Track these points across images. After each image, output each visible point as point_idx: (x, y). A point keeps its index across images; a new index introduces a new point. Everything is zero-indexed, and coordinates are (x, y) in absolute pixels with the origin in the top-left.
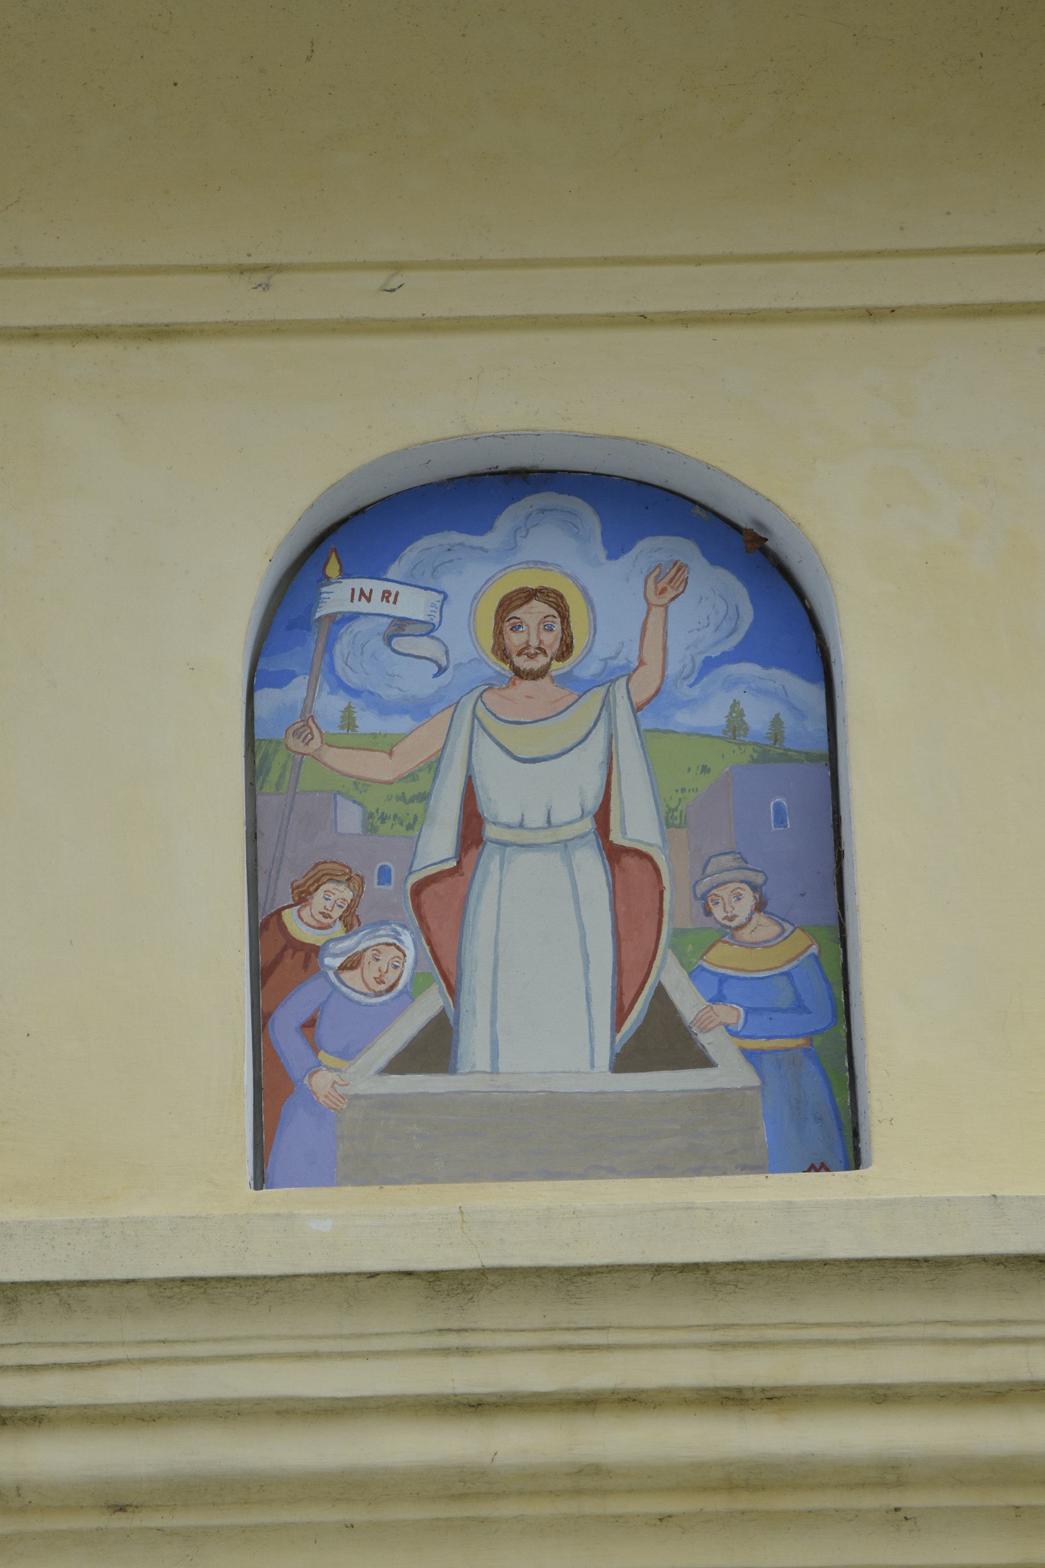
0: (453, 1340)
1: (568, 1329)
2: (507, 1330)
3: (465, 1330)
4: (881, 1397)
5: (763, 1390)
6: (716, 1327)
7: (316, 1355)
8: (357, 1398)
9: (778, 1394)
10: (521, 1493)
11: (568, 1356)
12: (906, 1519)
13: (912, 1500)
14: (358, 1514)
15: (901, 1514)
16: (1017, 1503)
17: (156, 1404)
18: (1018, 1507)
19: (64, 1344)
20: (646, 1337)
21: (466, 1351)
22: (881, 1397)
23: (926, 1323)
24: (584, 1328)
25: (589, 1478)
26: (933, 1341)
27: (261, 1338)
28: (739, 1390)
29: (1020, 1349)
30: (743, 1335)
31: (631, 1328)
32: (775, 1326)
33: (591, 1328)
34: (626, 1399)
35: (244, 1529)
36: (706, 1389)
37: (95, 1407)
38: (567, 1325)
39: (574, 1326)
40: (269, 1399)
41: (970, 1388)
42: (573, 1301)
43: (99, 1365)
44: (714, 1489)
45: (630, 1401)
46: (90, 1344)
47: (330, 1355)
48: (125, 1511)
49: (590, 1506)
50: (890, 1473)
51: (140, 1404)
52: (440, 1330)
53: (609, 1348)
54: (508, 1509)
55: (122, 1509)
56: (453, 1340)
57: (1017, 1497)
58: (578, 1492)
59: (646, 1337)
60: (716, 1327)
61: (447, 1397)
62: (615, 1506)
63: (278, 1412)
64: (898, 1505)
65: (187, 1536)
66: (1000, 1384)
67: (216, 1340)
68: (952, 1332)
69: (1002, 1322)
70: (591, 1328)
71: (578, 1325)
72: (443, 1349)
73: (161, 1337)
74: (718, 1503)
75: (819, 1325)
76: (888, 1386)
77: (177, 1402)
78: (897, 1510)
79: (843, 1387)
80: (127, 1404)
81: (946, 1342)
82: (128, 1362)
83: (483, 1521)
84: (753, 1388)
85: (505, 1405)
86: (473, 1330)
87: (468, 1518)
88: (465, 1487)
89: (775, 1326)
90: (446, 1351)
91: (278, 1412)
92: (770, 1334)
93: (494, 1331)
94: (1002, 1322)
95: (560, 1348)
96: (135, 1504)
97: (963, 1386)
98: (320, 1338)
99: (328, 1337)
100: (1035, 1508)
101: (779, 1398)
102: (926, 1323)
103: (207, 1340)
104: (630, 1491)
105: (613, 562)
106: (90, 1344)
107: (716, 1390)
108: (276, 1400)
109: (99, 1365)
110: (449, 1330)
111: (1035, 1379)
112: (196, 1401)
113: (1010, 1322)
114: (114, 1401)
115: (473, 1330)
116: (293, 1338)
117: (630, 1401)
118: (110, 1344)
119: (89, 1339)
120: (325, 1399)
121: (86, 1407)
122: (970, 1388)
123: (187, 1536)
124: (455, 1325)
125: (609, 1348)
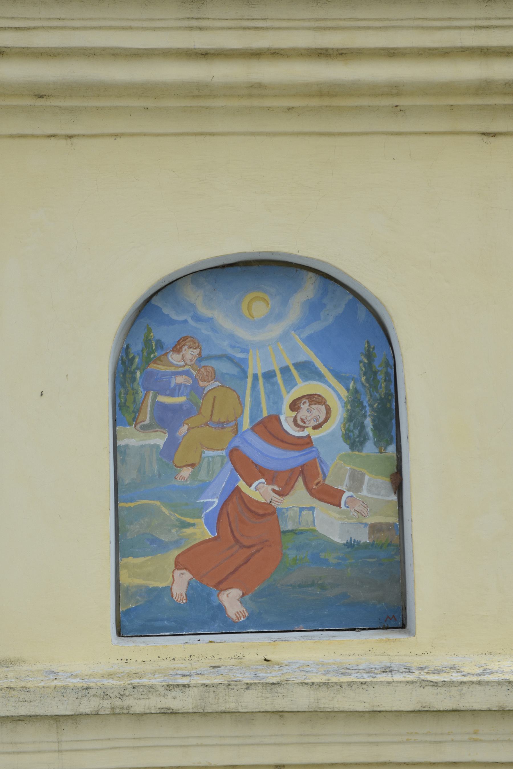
0: (194, 23)
1: (248, 19)
2: (220, 19)
3: (200, 18)
4: (392, 54)
5: (338, 50)
6: (317, 20)
7: (131, 28)
8: (149, 49)
9: (344, 52)
10: (225, 96)
11: (248, 32)
12: (401, 110)
13: (403, 102)
14: (150, 103)
15: (398, 108)
16: (451, 103)
17: (56, 48)
18: (452, 106)
19: (13, 18)
20: (285, 24)
21: (200, 29)
22: (392, 54)
23: (415, 19)
24: (256, 19)
25: (256, 89)
26: (417, 28)
27: (104, 19)
28: (327, 50)
29: (457, 31)
30: (330, 24)
31: (277, 19)
32: (345, 20)
33: (259, 19)
34: (274, 53)
35: (97, 108)
36: (311, 49)
37: (28, 48)
38: (248, 18)
39: (252, 18)
40: (108, 48)
41: (433, 50)
42: (250, 6)
43: (29, 29)
44: (313, 96)
45: (276, 54)
46: (25, 18)
47: (137, 28)
48: (43, 98)
49: (256, 102)
50: (395, 89)
51: (49, 48)
52: (188, 18)
53: (267, 28)
54: (219, 103)
55: (42, 97)
56: (194, 23)
57: (452, 101)
58: (250, 96)
59: (285, 24)
60: (317, 20)
61: (191, 50)
62: (269, 103)
63: (113, 55)
64: (397, 104)
65: (71, 110)
66: (447, 48)
67: (83, 19)
68: (426, 23)
69: (450, 19)
70: (259, 19)
71: (253, 18)
72: (189, 27)
73: (59, 17)
74: (315, 102)
75: (364, 19)
76: (395, 49)
77: (66, 48)
78: (396, 106)
79: (375, 49)
80: (42, 48)
81: (423, 28)
82: (43, 28)
83: (207, 108)
84: (333, 49)
85: (218, 54)
86: (204, 18)
87: (200, 106)
88: (199, 91)
89: (345, 20)
90: (191, 28)
91: (113, 55)
92: (342, 23)
93: (213, 19)
94: (450, 19)
95: (244, 28)
96: (47, 94)
97: (430, 49)
98: (132, 20)
99: (136, 20)
100: (459, 106)
101: (345, 54)
102: (415, 19)
103: (80, 19)
104: (275, 96)
105: (316, 431)
106: (25, 18)
107: (316, 49)
108: (112, 49)
109: (29, 29)
110: (193, 18)
111: (463, 46)
112: (75, 48)
113: (453, 19)
114: (36, 46)
115: (204, 18)
116: (120, 19)
117: (276, 54)
118: (34, 19)
119: (24, 16)
120: (135, 49)
121: (23, 48)
122: (433, 50)
123: (71, 110)
124: (196, 16)
125: (267, 28)
